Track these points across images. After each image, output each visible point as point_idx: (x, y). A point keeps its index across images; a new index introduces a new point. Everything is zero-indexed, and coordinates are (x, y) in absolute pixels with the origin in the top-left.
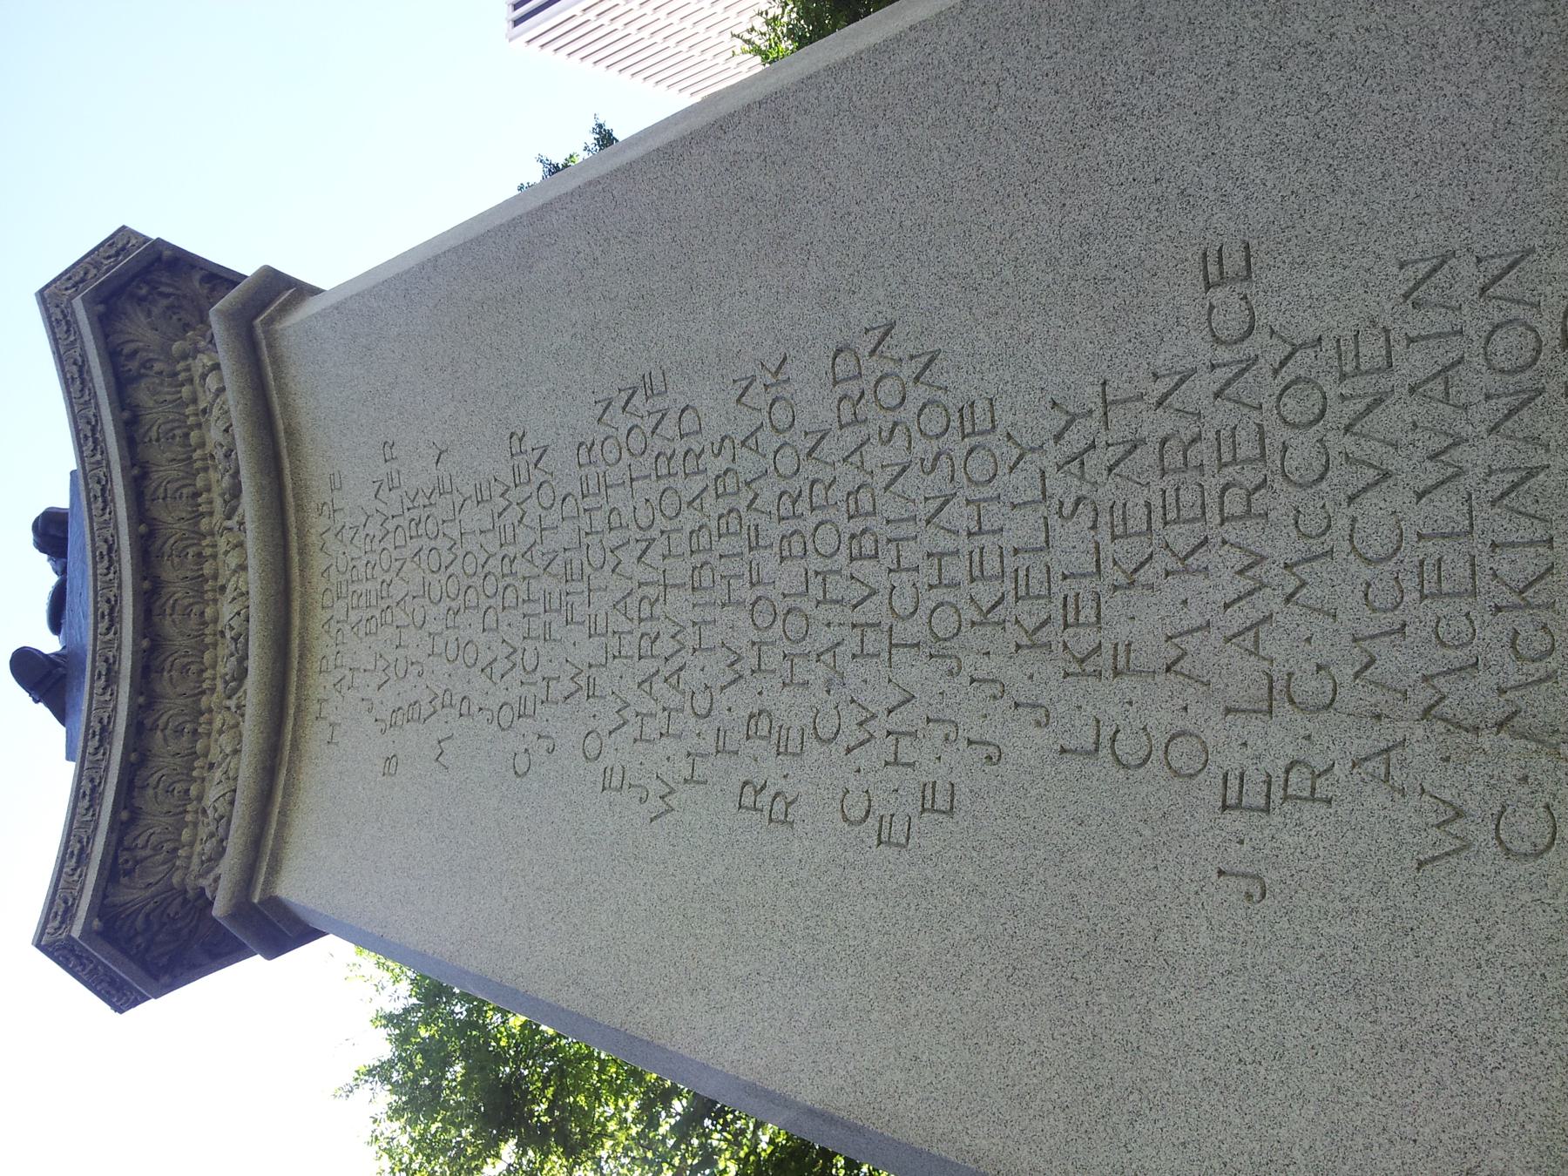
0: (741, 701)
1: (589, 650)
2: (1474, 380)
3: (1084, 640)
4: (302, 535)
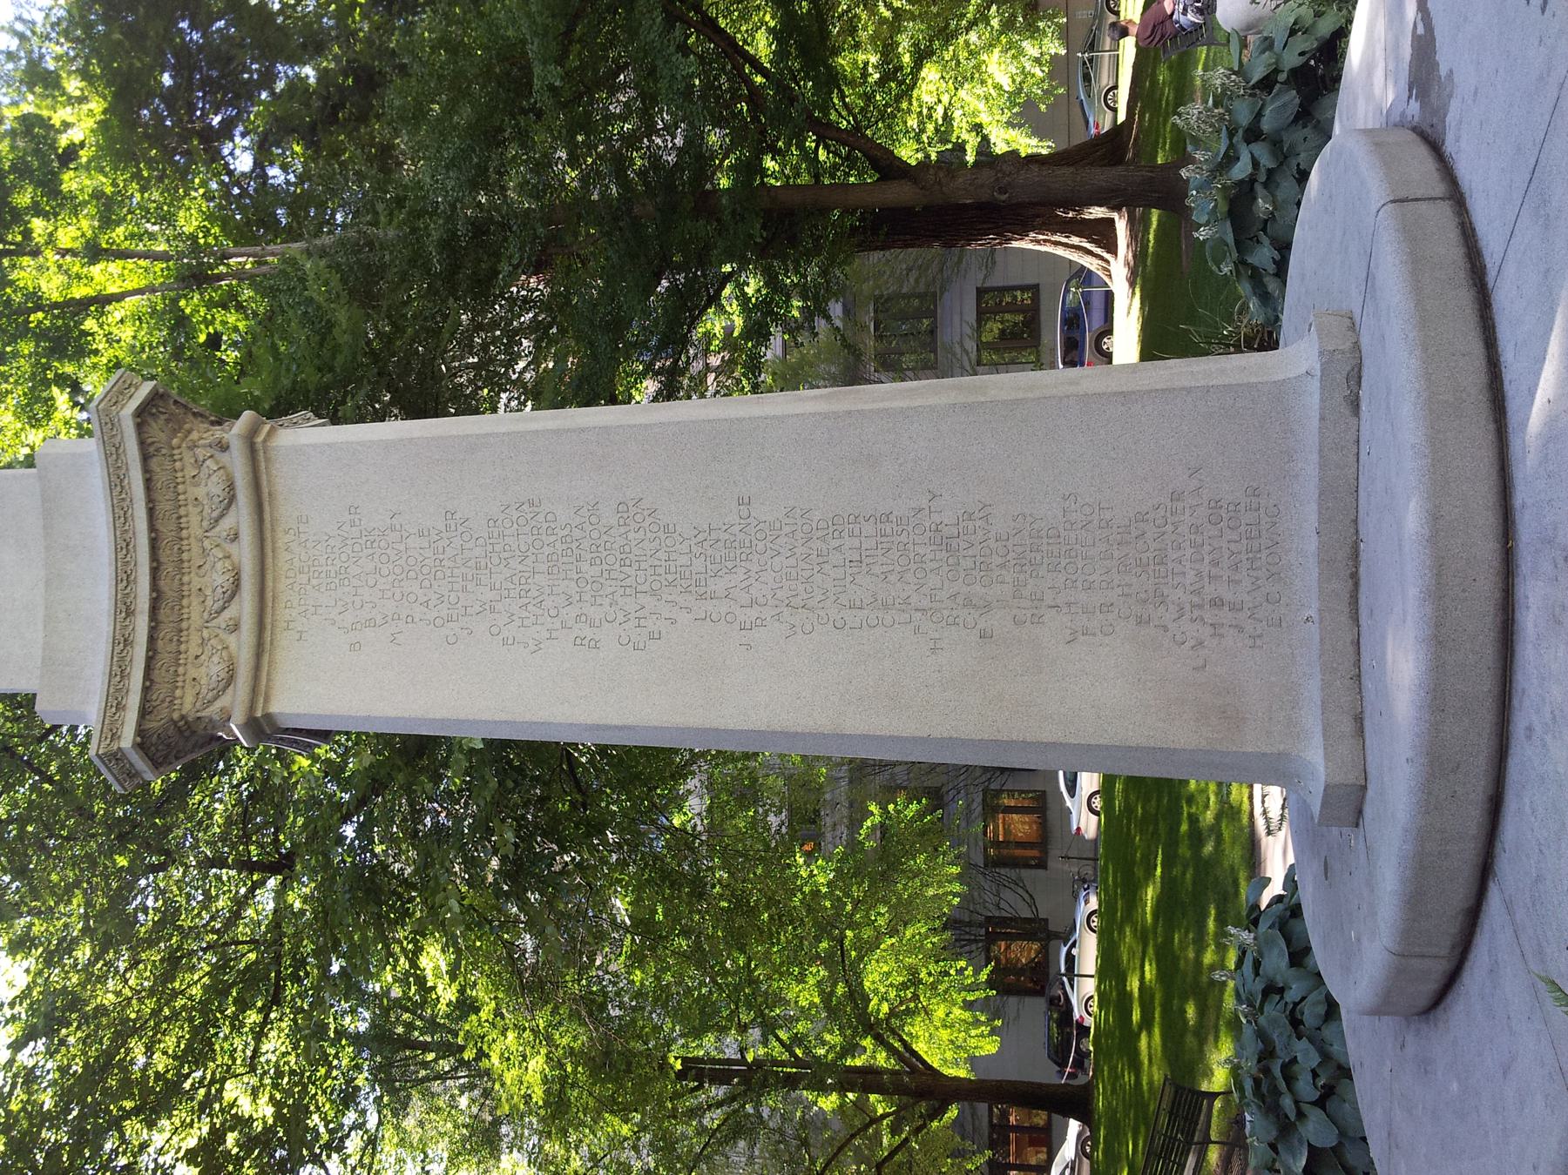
0: (573, 611)
1: (490, 595)
2: (799, 535)
3: (702, 590)
4: (274, 543)
